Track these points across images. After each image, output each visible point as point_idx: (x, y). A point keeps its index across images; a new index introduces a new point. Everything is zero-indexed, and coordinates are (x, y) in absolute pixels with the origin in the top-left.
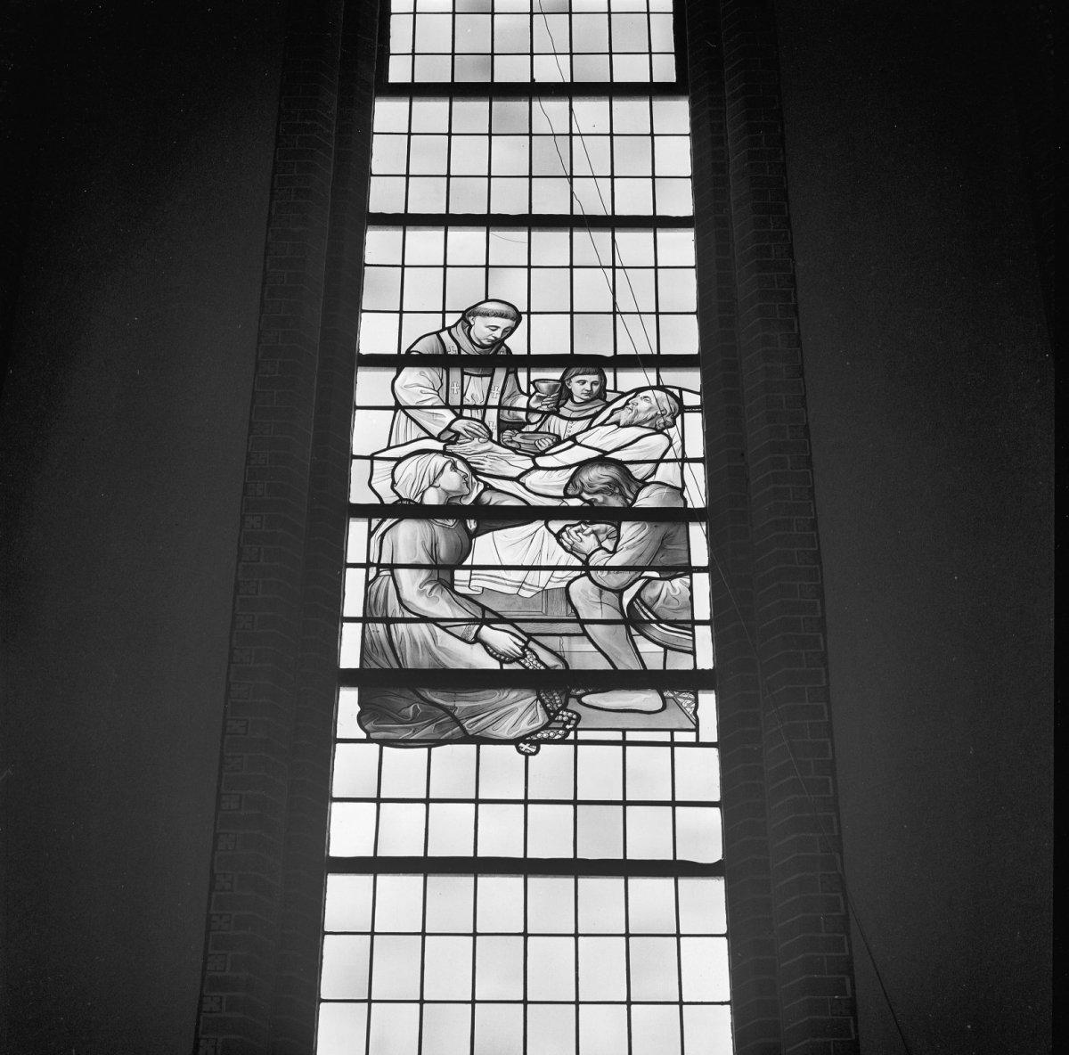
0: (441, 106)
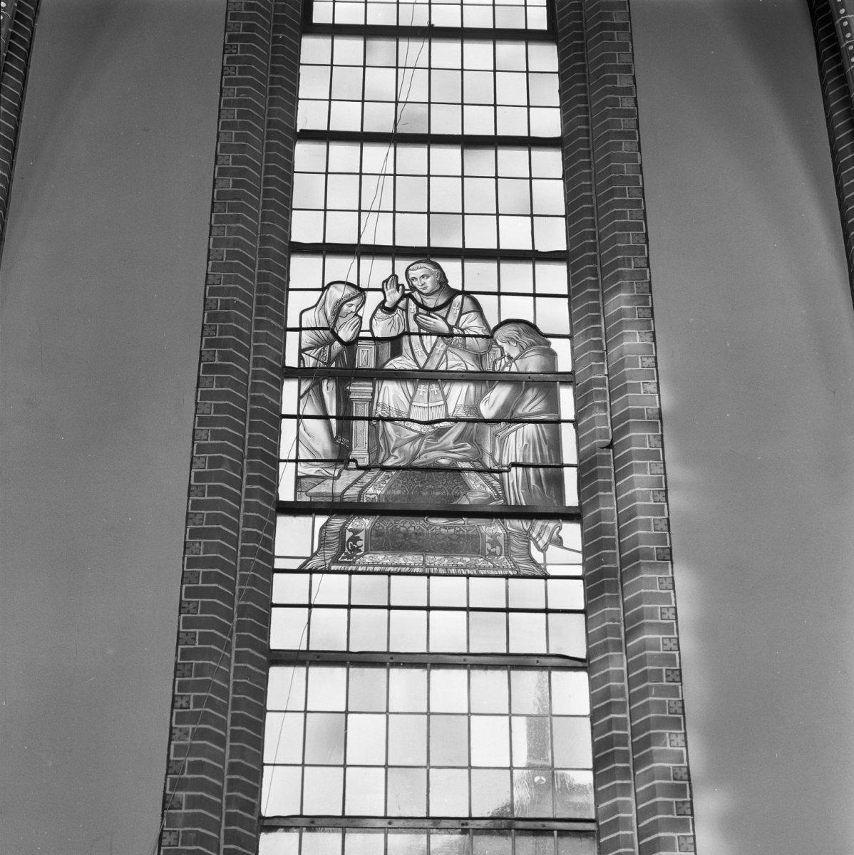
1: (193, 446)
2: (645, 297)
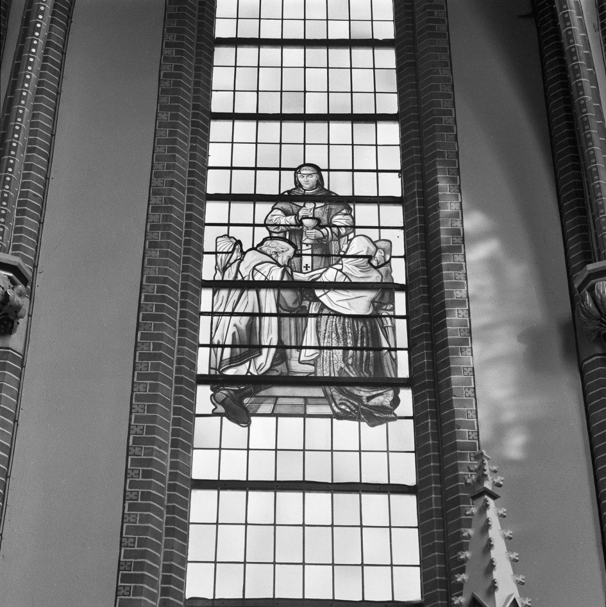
0: (345, 52)
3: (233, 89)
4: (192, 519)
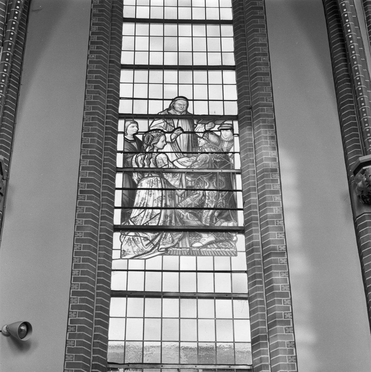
1: (89, 42)
2: (273, 126)
3: (134, 84)
4: (111, 314)
